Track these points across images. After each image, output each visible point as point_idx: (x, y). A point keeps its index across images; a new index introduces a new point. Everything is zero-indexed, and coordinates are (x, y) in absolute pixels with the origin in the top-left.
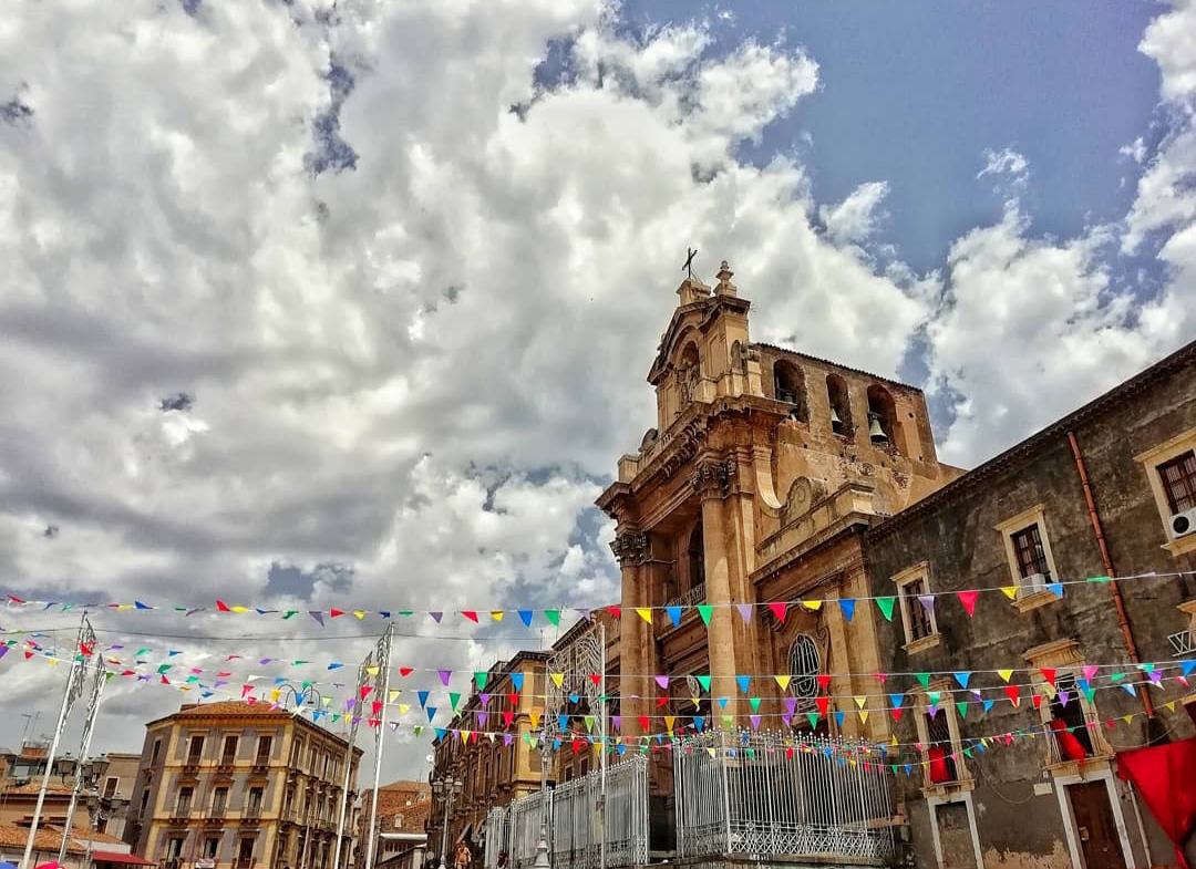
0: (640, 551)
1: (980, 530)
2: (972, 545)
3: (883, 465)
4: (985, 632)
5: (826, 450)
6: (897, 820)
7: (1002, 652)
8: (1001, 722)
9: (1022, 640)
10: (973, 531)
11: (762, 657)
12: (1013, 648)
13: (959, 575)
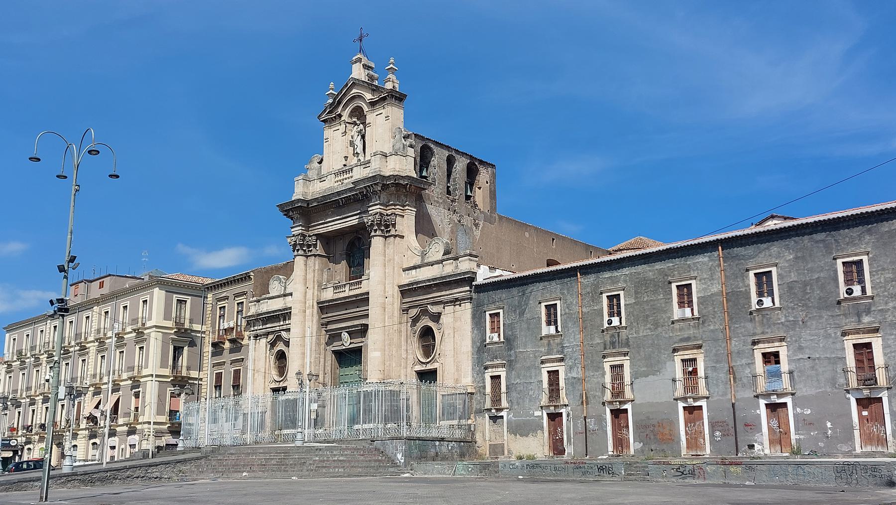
0: (309, 246)
4: (525, 346)
6: (470, 422)
9: (541, 352)
10: (529, 298)
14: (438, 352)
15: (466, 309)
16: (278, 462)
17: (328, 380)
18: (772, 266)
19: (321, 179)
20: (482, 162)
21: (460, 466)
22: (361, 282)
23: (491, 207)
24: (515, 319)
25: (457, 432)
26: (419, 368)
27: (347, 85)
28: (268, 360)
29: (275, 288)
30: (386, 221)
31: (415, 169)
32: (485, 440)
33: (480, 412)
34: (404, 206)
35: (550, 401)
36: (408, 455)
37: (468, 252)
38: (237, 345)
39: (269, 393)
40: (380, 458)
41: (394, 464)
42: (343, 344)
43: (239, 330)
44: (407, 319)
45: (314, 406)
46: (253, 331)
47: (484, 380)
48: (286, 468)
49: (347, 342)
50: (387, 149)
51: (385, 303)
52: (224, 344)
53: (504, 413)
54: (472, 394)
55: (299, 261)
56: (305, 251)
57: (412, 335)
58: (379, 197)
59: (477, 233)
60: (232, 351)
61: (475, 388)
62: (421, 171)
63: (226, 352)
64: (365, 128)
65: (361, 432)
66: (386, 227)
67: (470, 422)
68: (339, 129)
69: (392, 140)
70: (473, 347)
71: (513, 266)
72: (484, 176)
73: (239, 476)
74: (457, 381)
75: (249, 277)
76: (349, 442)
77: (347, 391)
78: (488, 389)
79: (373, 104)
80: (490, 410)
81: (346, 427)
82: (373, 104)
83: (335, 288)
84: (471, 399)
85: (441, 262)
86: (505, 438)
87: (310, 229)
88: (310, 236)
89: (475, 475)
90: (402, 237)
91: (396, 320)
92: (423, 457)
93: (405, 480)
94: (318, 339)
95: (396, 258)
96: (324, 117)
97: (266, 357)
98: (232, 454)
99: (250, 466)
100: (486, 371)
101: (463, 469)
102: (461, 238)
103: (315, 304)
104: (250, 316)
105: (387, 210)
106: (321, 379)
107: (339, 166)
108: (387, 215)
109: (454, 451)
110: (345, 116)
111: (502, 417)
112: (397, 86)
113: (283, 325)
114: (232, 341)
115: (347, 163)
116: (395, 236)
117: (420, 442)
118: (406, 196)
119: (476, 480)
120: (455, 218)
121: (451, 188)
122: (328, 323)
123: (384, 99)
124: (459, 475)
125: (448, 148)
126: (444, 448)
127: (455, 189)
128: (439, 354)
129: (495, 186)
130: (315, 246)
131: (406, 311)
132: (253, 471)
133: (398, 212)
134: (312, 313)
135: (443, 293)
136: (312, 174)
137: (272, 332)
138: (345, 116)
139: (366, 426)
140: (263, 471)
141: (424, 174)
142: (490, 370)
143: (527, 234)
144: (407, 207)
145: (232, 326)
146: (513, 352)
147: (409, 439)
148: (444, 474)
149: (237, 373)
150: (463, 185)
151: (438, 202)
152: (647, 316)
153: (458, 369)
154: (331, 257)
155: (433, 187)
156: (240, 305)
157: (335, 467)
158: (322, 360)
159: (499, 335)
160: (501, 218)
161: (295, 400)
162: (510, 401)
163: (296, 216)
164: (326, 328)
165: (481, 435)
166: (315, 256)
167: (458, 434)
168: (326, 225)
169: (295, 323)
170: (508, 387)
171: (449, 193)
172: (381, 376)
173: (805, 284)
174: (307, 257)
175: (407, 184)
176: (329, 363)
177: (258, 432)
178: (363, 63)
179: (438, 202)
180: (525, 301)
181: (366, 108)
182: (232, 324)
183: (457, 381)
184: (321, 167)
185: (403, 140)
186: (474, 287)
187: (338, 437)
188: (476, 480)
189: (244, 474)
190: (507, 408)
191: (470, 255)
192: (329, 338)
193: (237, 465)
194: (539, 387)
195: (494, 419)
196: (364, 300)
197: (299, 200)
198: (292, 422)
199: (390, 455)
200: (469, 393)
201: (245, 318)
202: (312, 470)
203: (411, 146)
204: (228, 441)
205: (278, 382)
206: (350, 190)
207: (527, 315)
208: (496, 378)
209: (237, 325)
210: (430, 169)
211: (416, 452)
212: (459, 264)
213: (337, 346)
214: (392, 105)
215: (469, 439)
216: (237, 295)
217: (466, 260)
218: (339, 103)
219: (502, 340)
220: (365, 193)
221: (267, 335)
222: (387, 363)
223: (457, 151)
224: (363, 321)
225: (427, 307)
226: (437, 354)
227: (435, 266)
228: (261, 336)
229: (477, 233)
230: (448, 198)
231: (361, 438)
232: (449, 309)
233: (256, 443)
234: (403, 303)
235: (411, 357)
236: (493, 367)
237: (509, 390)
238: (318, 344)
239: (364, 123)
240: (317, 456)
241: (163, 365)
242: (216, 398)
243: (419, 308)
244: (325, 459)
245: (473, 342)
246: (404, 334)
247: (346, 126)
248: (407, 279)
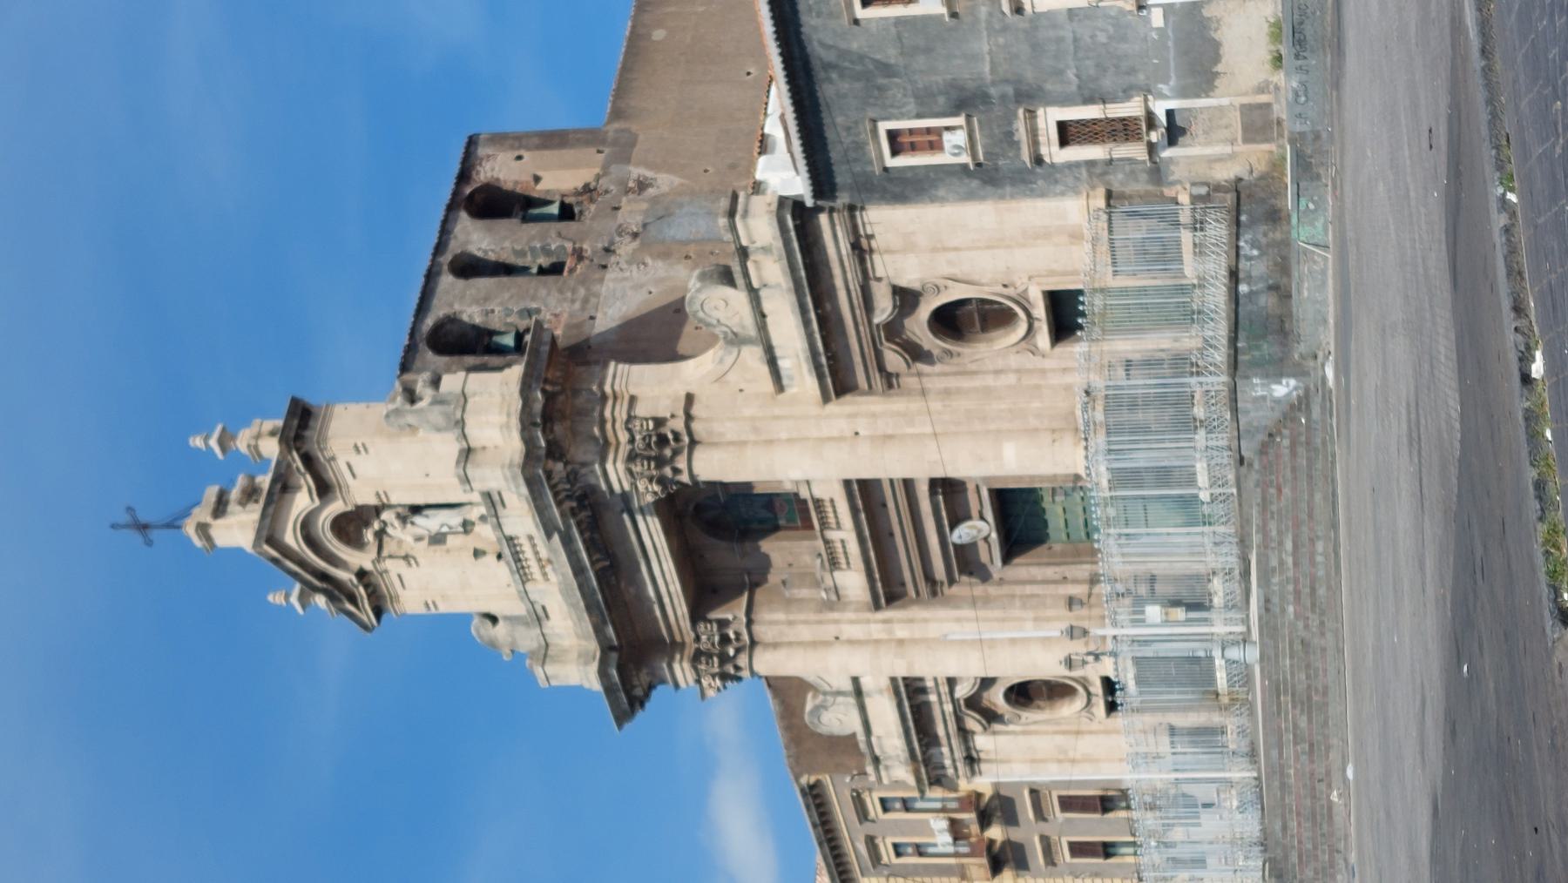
0: (725, 640)
1: (843, 45)
2: (861, 58)
3: (617, 209)
4: (975, 58)
5: (596, 288)
6: (1184, 199)
7: (1001, 40)
8: (1080, 55)
9: (990, 14)
10: (844, 54)
11: (947, 393)
12: (997, 26)
13: (896, 80)
14: (1000, 289)
15: (881, 219)
16: (1302, 710)
17: (1083, 571)
18: (875, 131)
19: (539, 617)
20: (464, 176)
21: (1303, 233)
22: (818, 503)
23: (588, 143)
24: (905, 89)
25: (1213, 232)
26: (1043, 338)
27: (275, 561)
28: (1033, 728)
29: (840, 719)
30: (649, 445)
31: (499, 369)
32: (1232, 157)
33: (1157, 172)
34: (604, 398)
35: (1140, 139)
36: (1277, 368)
37: (723, 221)
38: (995, 808)
39: (1119, 720)
40: (1286, 442)
41: (1301, 404)
42: (986, 539)
43: (954, 805)
44: (912, 375)
45: (1153, 612)
46: (956, 769)
47: (1072, 166)
48: (1317, 690)
49: (979, 529)
50: (448, 446)
51: (873, 439)
52: (992, 842)
53: (1160, 109)
54: (1109, 195)
55: (767, 663)
56: (738, 651)
57: (955, 360)
58: (584, 464)
59: (665, 182)
60: (1011, 818)
61: (1093, 188)
62: (501, 350)
63: (1016, 835)
64: (390, 507)
65: (1220, 490)
67: (1184, 199)
68: (399, 576)
69: (421, 433)
70: (983, 198)
71: (749, 74)
72: (500, 169)
73: (1339, 811)
74: (1075, 236)
75: (812, 787)
76: (1244, 522)
77: (1112, 531)
79: (324, 489)
80: (1152, 148)
81: (1207, 529)
82: (324, 489)
83: (834, 564)
84: (1123, 197)
85: (754, 295)
86: (1225, 101)
87: (678, 638)
88: (698, 639)
89: (1326, 192)
90: (690, 399)
91: (915, 405)
92: (1280, 327)
93: (1343, 369)
94: (973, 602)
95: (747, 412)
96: (368, 615)
97: (1024, 733)
98: (1285, 828)
99: (1317, 782)
100: (1047, 159)
101: (1312, 224)
102: (680, 229)
103: (881, 615)
104: (919, 780)
105: (618, 443)
106: (1079, 590)
107: (502, 572)
108: (632, 441)
109: (1263, 241)
110: (361, 559)
111: (1170, 114)
112: (269, 425)
113: (939, 695)
114: (985, 819)
115: (492, 550)
116: (689, 418)
117: (1242, 335)
118: (576, 392)
119: (1339, 198)
120: (626, 248)
121: (544, 261)
122: (930, 578)
123: (309, 461)
124: (1326, 234)
125: (431, 276)
126: (1256, 267)
127: (546, 251)
128: (1005, 286)
129: (528, 135)
130: (723, 624)
131: (890, 380)
132: (1328, 773)
133: (621, 414)
134: (901, 621)
135: (839, 282)
136: (528, 640)
137: (959, 720)
138: (361, 559)
139: (1202, 479)
140: (1328, 748)
141: (509, 340)
142: (1044, 151)
143: (658, 34)
144: (608, 389)
145: (944, 824)
146: (993, 91)
147: (1234, 365)
148: (1324, 272)
149: (1068, 804)
150: (533, 229)
151: (586, 301)
153: (1044, 235)
154: (752, 579)
155: (546, 316)
156: (901, 850)
157: (1313, 563)
158: (1029, 589)
159: (948, 129)
160: (617, 114)
161: (1137, 661)
162: (1126, 94)
163: (644, 677)
164: (942, 583)
165: (1217, 166)
166: (750, 623)
167: (1218, 230)
168: (666, 600)
169: (930, 667)
170: (1088, 100)
171: (556, 269)
172: (1069, 438)
174: (753, 643)
175: (544, 391)
176: (1037, 572)
177: (1225, 750)
178: (209, 519)
179: (586, 301)
180: (852, 62)
181: (336, 507)
182: (939, 824)
183: (1075, 236)
184: (507, 618)
185: (420, 405)
186: (819, 203)
187: (1235, 550)
188: (1339, 198)
189: (1334, 797)
190: (1146, 100)
191: (732, 214)
192: (971, 574)
193: (1314, 815)
194: (1087, 17)
195: (1175, 132)
196: (865, 494)
197: (603, 673)
198: (1195, 672)
199: (1277, 415)
200: (1108, 205)
201: (922, 792)
202: (1322, 623)
203: (436, 382)
204: (1250, 825)
205: (1089, 701)
206: (567, 542)
207: (891, 55)
208: (1067, 134)
209: (944, 810)
210: (495, 323)
211: (1268, 348)
212: (758, 244)
213: (991, 554)
214: (322, 439)
215: (1230, 198)
216: (862, 814)
217: (747, 227)
218: (324, 577)
219: (960, 120)
220: (574, 504)
221: (965, 734)
222: (1033, 422)
223: (440, 248)
224: (923, 491)
225: (878, 326)
226: (1006, 291)
227: (767, 306)
228: (968, 749)
230: (572, 271)
231: (1234, 491)
232: (883, 266)
233: (1252, 754)
234: (870, 386)
235: (1014, 361)
236: (1035, 143)
237: (1097, 95)
238: (987, 601)
239: (378, 510)
240: (1283, 611)
242: (1135, 854)
243: (881, 343)
244: (1290, 588)
245: (970, 196)
246: (952, 383)
247: (391, 557)
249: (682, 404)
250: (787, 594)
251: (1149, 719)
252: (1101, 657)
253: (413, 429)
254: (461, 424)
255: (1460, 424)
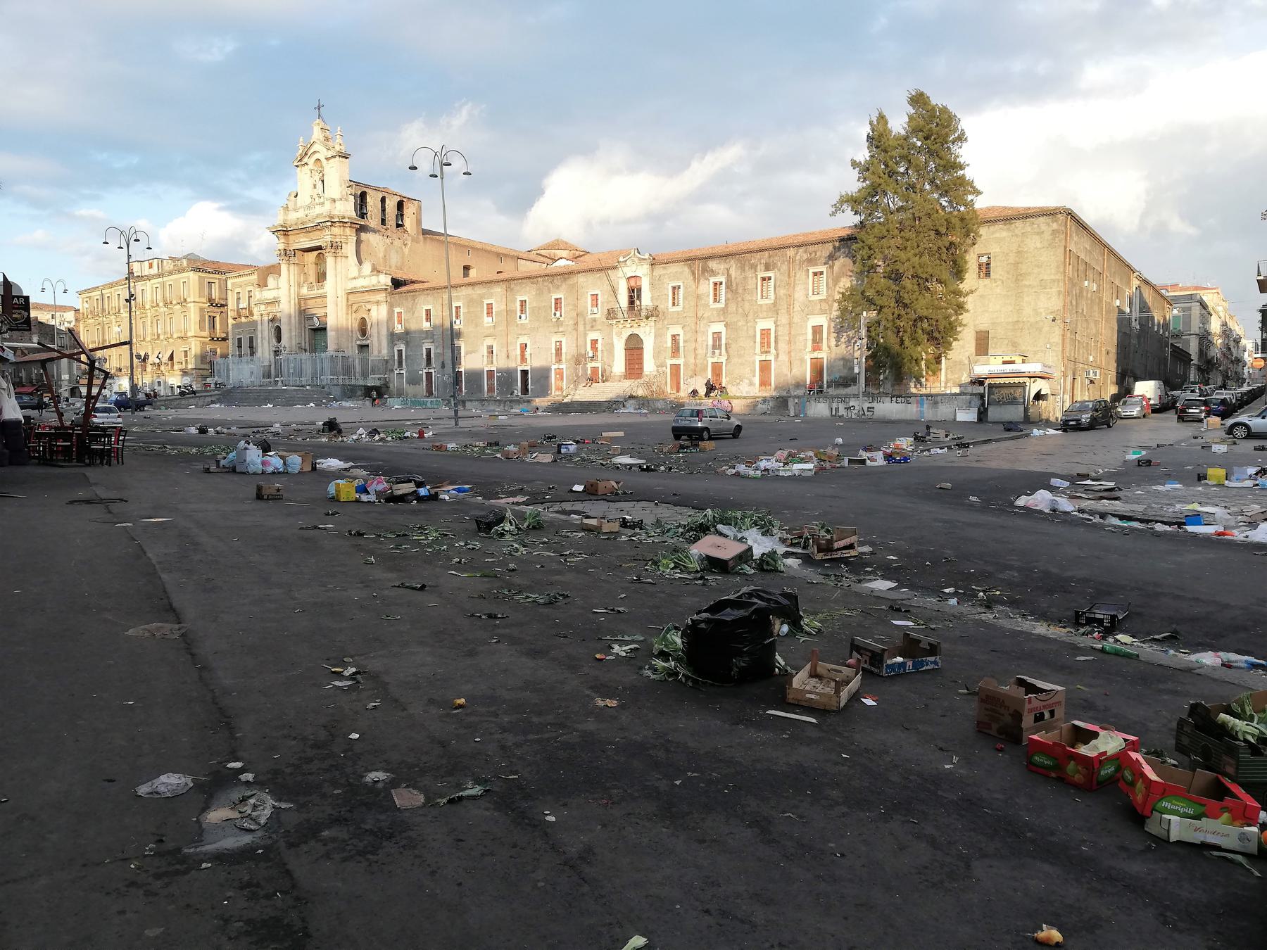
2: (416, 308)
26: (358, 343)
29: (271, 281)
50: (336, 196)
66: (335, 247)
72: (409, 210)
78: (396, 358)
107: (308, 200)
120: (388, 241)
149: (251, 339)
152: (472, 320)
158: (303, 334)
173: (539, 308)
207: (416, 314)
229: (406, 251)
241: (201, 329)
248: (352, 285)
249: (345, 255)
250: (302, 275)
251: (273, 360)
252: (834, 209)
253: (341, 186)
254: (341, 199)
255: (1039, 635)
